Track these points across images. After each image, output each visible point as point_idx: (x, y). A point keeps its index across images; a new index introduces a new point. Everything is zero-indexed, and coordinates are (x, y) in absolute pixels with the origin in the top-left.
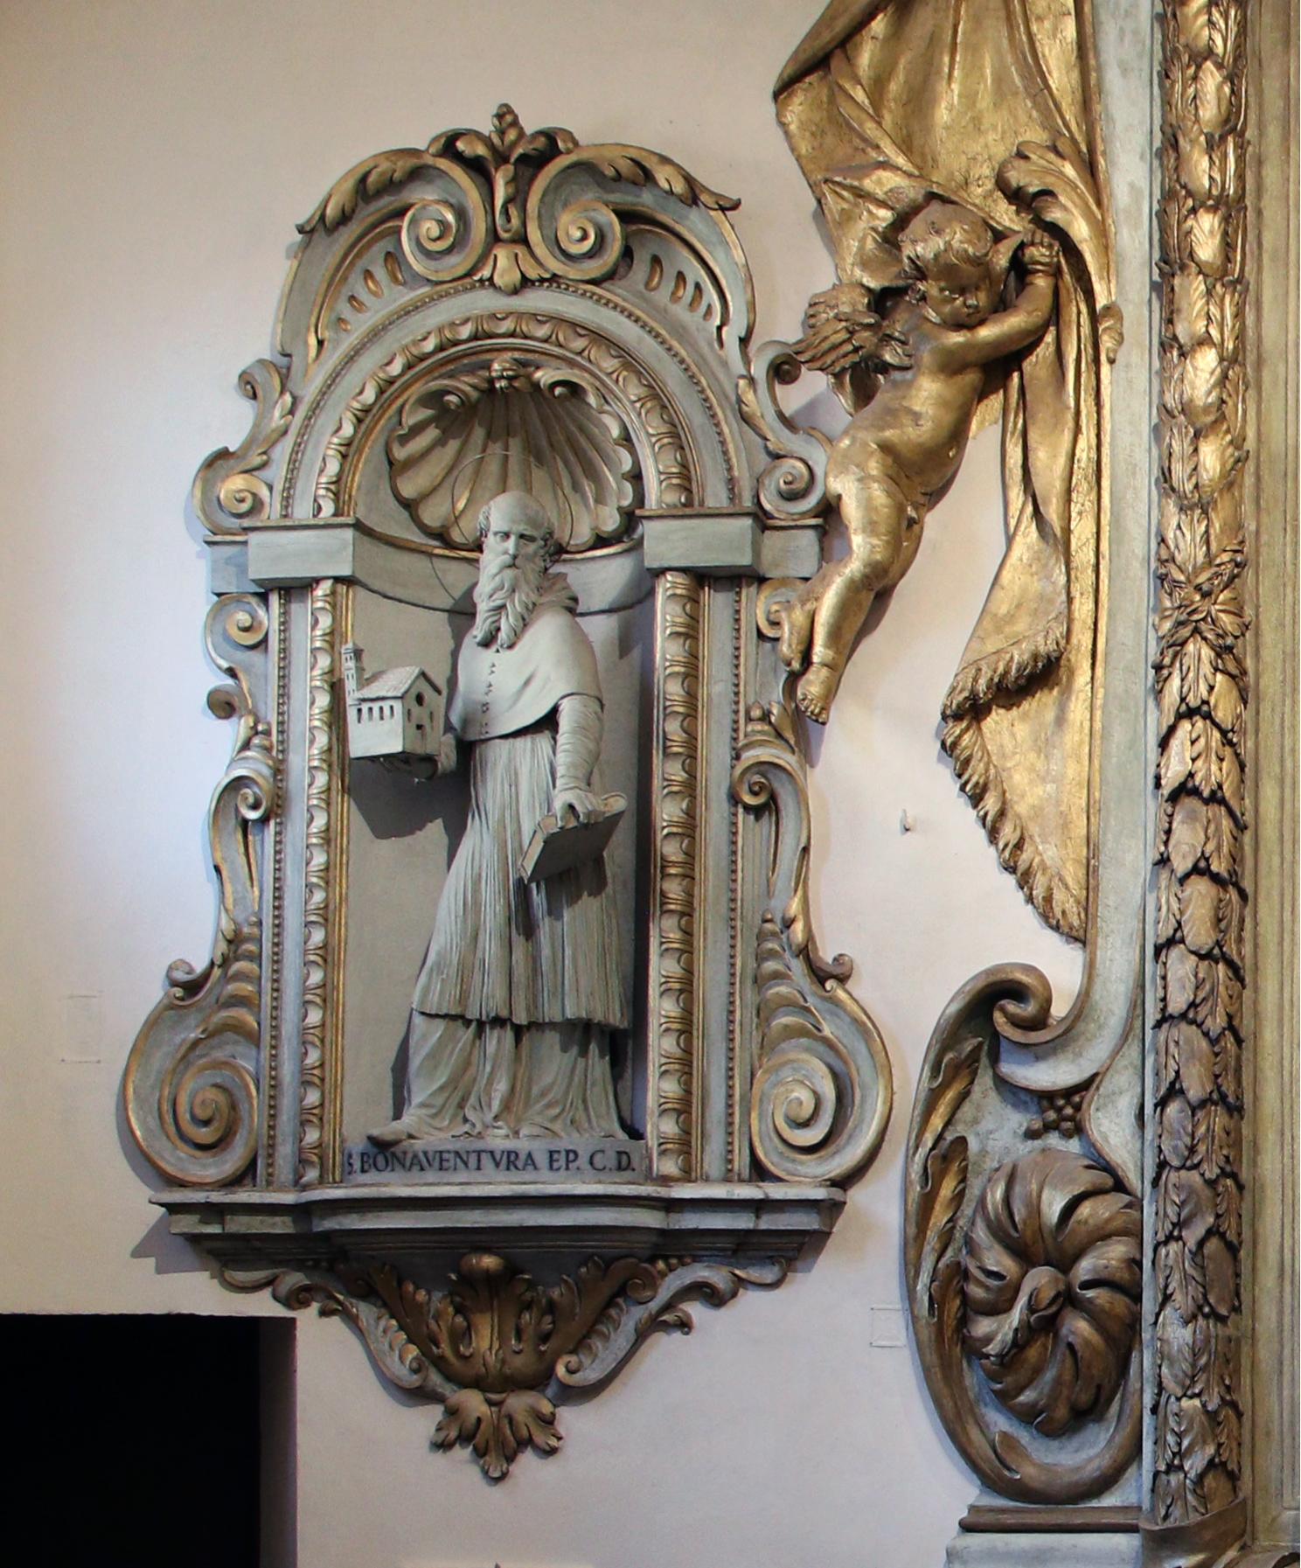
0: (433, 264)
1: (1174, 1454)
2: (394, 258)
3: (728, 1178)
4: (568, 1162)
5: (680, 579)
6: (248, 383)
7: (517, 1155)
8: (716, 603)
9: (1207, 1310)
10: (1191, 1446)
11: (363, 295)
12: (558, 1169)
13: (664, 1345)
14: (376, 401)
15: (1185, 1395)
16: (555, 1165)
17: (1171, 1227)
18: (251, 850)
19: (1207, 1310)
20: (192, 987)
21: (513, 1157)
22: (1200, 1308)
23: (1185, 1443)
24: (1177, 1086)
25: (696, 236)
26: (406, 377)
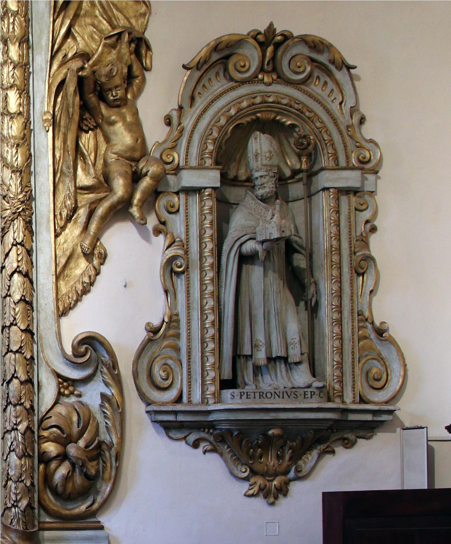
0: (234, 70)
1: (14, 501)
2: (226, 70)
3: (354, 402)
4: (311, 395)
5: (210, 190)
6: (169, 119)
7: (263, 393)
8: (344, 199)
9: (26, 454)
10: (20, 499)
11: (207, 84)
12: (308, 398)
13: (328, 458)
14: (226, 124)
15: (18, 481)
16: (306, 396)
17: (13, 425)
18: (363, 289)
19: (26, 454)
20: (155, 331)
21: (261, 394)
22: (24, 453)
23: (18, 498)
24: (15, 375)
25: (49, 47)
26: (305, 118)
